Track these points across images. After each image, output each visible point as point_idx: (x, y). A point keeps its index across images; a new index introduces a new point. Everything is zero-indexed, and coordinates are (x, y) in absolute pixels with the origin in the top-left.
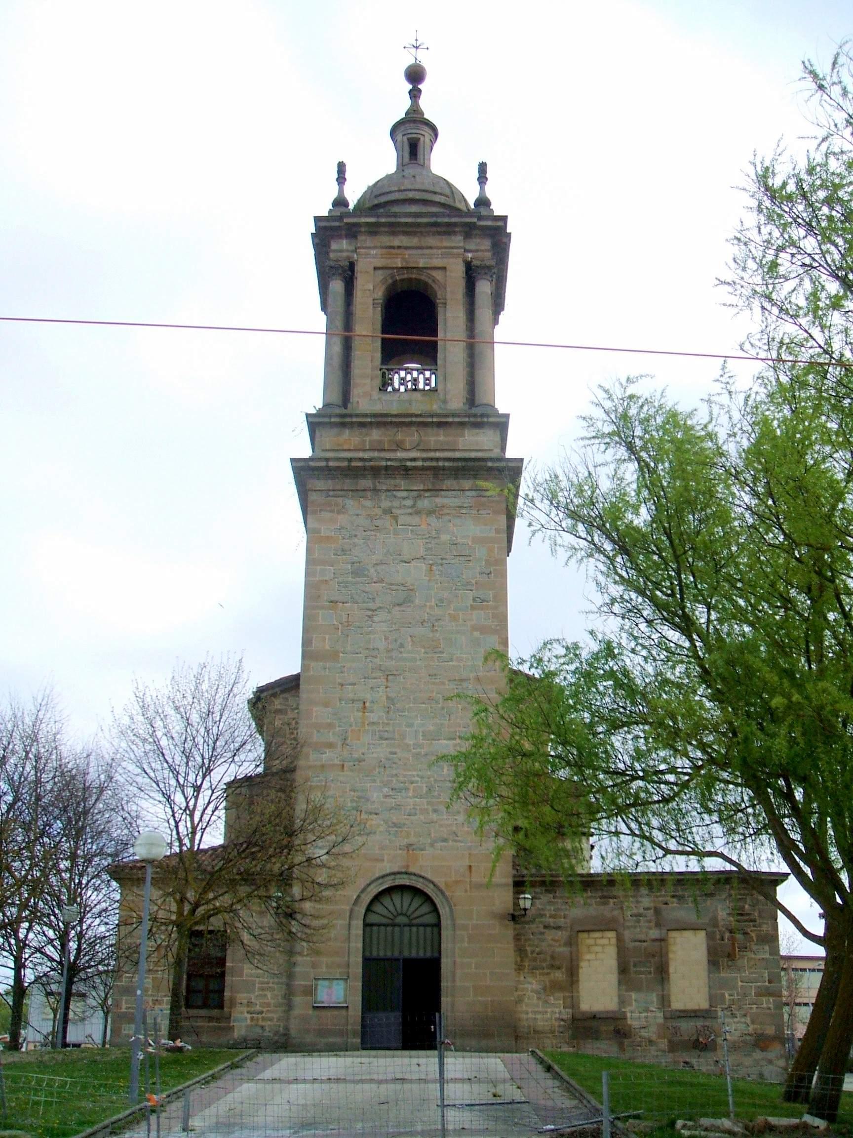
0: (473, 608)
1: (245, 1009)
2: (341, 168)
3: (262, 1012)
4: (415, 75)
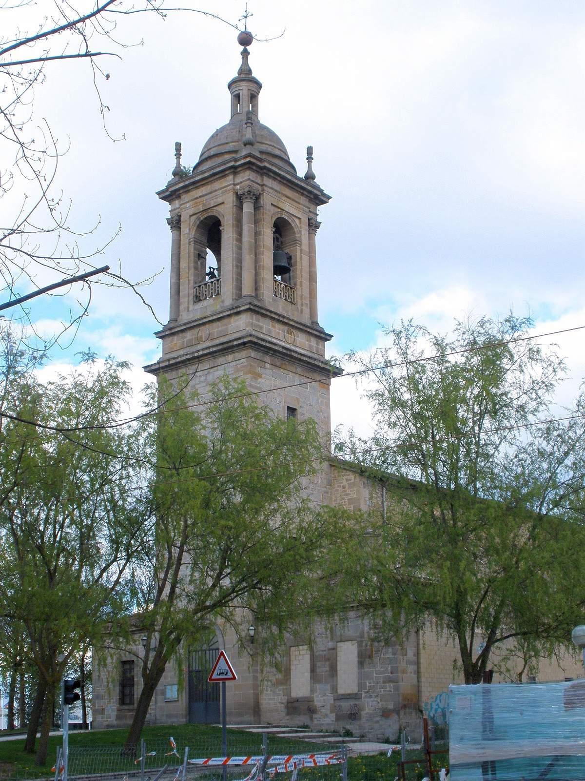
2: (178, 147)
4: (245, 40)
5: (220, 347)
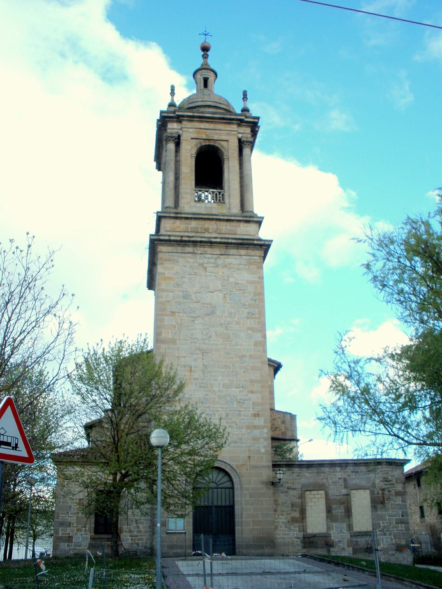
0: (248, 318)
1: (128, 534)
2: (173, 89)
3: (137, 536)
4: (205, 49)
5: (240, 241)
